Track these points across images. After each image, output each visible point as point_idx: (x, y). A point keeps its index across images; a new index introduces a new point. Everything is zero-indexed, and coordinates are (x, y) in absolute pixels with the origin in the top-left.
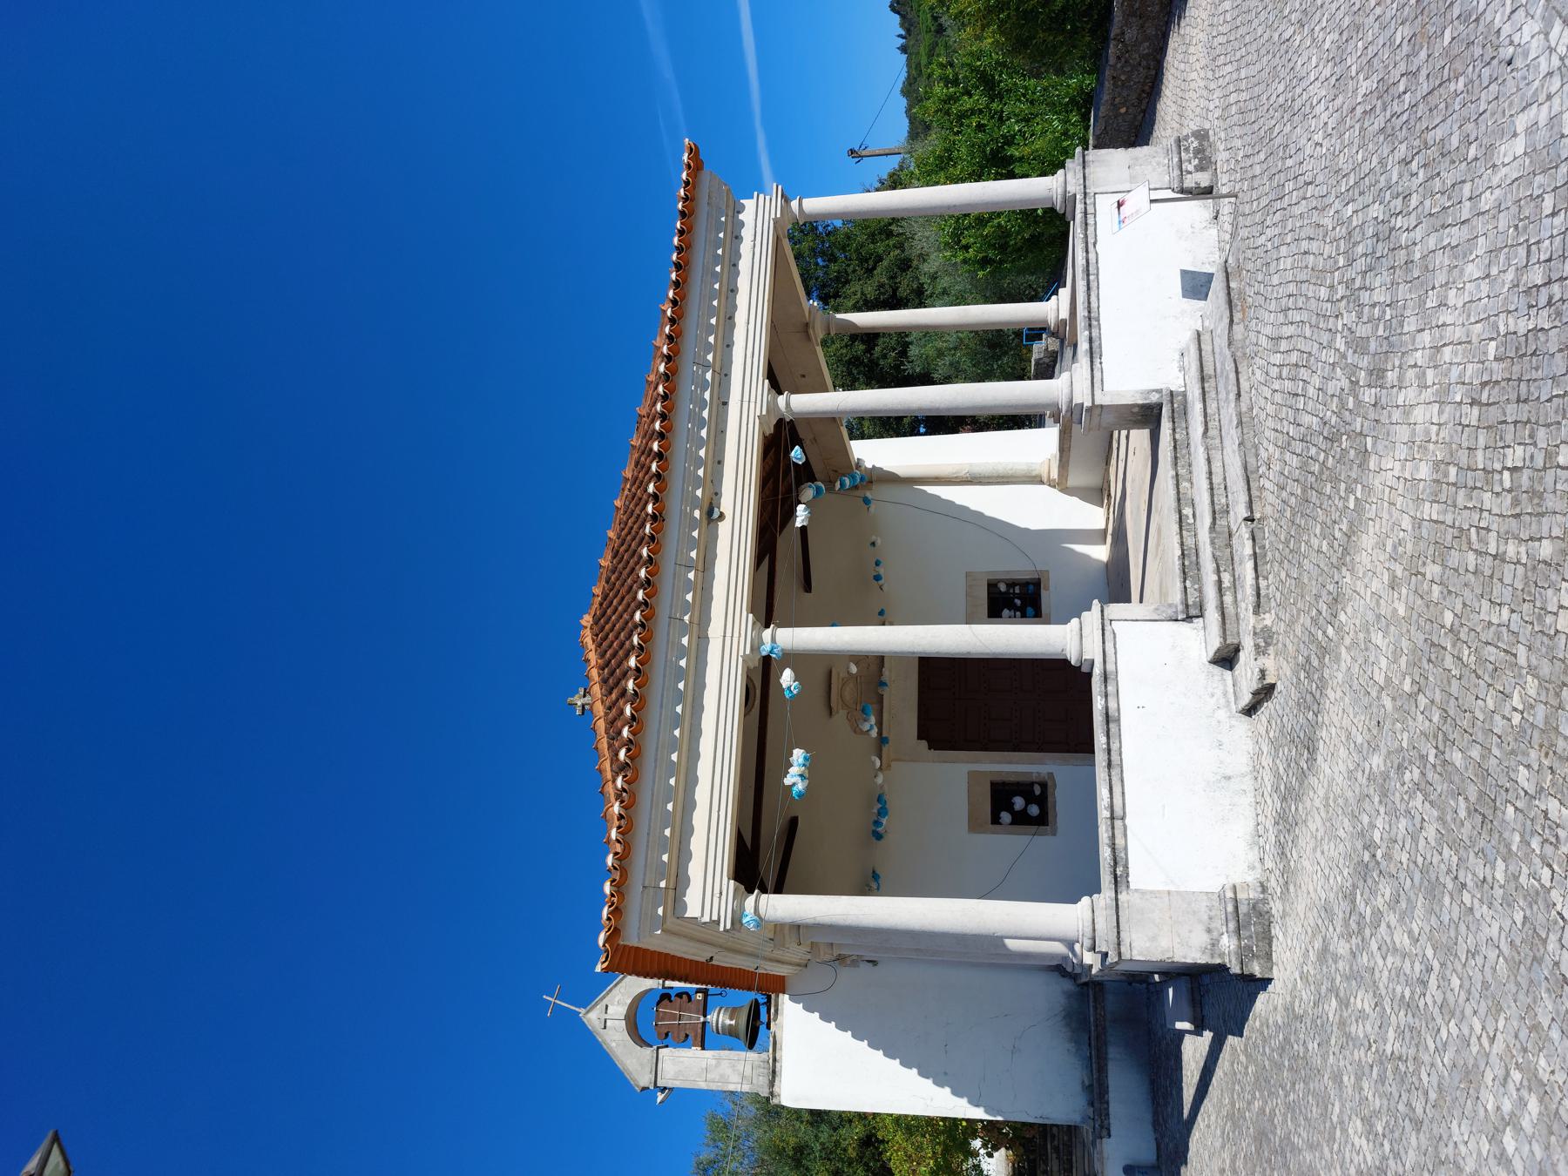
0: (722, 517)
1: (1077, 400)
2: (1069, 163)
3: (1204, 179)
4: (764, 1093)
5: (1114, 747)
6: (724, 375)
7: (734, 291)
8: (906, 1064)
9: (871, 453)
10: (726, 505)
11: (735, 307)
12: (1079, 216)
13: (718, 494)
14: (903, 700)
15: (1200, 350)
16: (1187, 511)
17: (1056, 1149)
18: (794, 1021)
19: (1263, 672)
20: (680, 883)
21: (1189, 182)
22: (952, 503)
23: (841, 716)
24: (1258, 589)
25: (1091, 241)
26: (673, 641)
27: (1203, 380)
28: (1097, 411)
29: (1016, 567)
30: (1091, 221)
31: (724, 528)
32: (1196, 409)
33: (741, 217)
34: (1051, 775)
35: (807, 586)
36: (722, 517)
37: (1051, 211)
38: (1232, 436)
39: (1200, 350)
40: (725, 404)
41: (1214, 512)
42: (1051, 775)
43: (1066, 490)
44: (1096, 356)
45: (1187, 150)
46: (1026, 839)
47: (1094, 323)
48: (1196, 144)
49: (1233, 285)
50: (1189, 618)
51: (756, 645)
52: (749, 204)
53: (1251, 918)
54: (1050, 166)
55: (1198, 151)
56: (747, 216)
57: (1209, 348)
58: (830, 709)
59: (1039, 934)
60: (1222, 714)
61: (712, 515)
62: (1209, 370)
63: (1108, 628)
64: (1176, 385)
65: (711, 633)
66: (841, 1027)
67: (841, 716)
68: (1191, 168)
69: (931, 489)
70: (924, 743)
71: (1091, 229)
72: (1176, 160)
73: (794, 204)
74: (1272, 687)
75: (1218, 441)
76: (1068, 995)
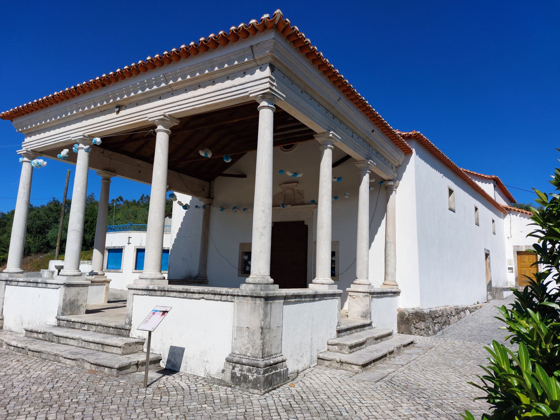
6: (172, 92)
7: (214, 83)
8: (182, 224)
10: (122, 113)
11: (204, 87)
13: (126, 108)
15: (114, 346)
16: (86, 327)
22: (376, 234)
24: (11, 346)
25: (206, 296)
26: (70, 108)
27: (102, 344)
30: (217, 297)
31: (114, 115)
33: (258, 71)
36: (118, 112)
39: (114, 346)
40: (160, 98)
41: (59, 337)
44: (145, 293)
45: (249, 371)
46: (237, 267)
47: (163, 293)
48: (251, 378)
49: (106, 369)
55: (245, 378)
56: (258, 74)
57: (114, 352)
59: (101, 263)
61: (120, 107)
62: (106, 349)
63: (58, 286)
65: (84, 122)
68: (237, 370)
69: (384, 222)
71: (212, 297)
72: (244, 361)
73: (264, 103)
75: (80, 345)
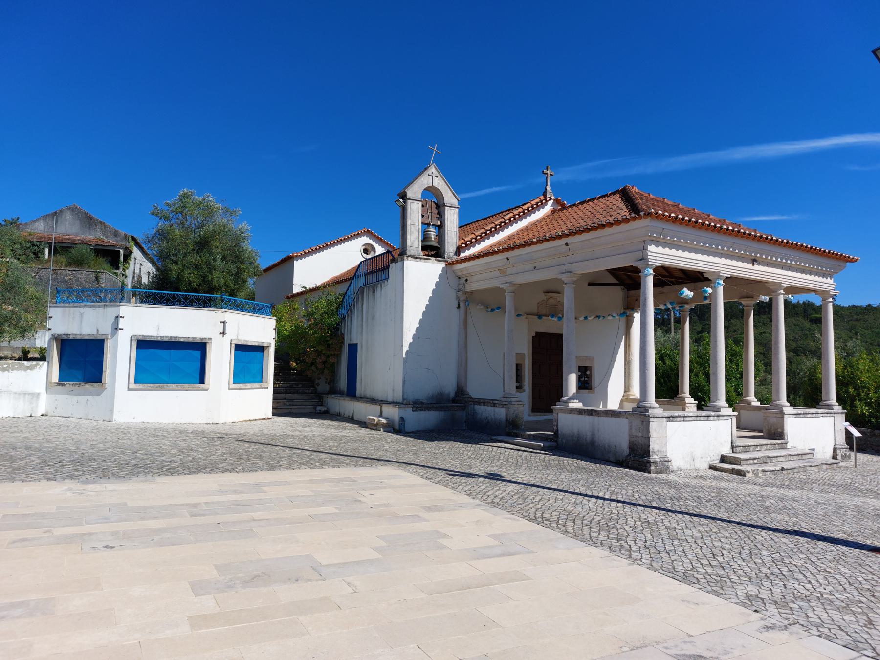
0: (753, 265)
1: (651, 411)
2: (731, 409)
3: (839, 457)
4: (408, 253)
5: (701, 418)
9: (637, 316)
10: (756, 267)
12: (820, 411)
14: (548, 326)
16: (759, 448)
17: (291, 386)
18: (434, 269)
19: (748, 472)
20: (665, 245)
21: (838, 451)
23: (543, 297)
28: (779, 416)
29: (596, 380)
31: (750, 266)
32: (783, 452)
34: (524, 391)
35: (590, 284)
37: (821, 400)
38: (801, 464)
42: (524, 391)
43: (622, 401)
50: (732, 447)
51: (718, 275)
52: (832, 281)
53: (664, 466)
54: (839, 399)
56: (830, 281)
58: (548, 292)
60: (709, 459)
61: (754, 261)
62: (804, 457)
64: (789, 446)
66: (434, 291)
67: (543, 297)
70: (534, 335)
74: (744, 475)
76: (448, 395)
